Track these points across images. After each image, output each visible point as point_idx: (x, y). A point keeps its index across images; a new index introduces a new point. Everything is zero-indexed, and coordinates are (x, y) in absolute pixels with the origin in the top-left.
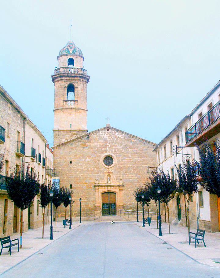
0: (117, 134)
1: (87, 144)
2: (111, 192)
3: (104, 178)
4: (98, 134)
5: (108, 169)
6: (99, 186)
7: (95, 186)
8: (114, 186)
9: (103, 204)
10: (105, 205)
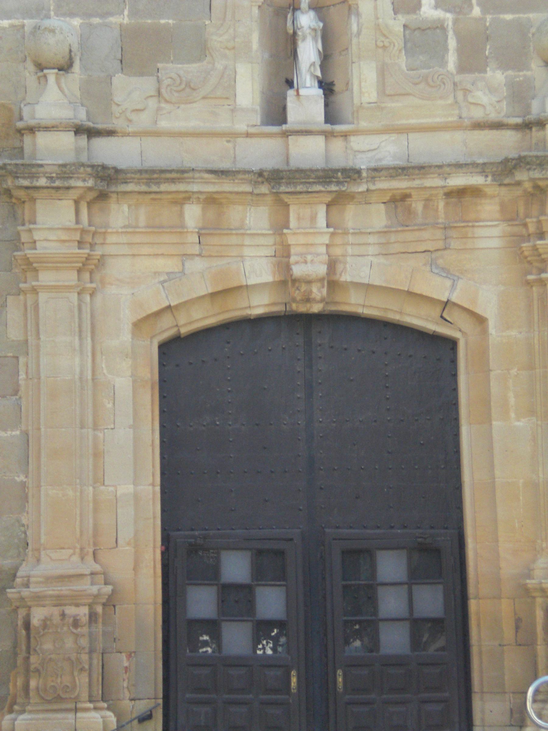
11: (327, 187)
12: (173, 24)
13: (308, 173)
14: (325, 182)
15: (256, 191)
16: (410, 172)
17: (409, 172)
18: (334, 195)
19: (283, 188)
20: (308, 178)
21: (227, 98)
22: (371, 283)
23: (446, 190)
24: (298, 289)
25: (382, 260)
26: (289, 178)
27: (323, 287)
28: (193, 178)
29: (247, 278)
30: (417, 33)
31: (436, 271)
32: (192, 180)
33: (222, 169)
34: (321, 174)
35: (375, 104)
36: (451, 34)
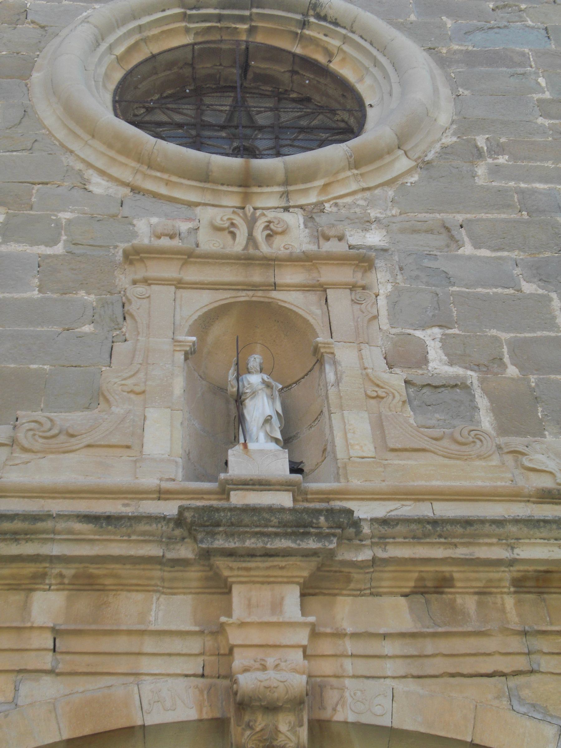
11: (301, 543)
12: (50, 369)
13: (266, 516)
14: (293, 534)
15: (170, 555)
16: (447, 529)
17: (445, 529)
18: (313, 563)
19: (220, 543)
20: (266, 526)
21: (128, 447)
22: (397, 725)
23: (516, 571)
24: (249, 726)
25: (412, 686)
26: (232, 524)
27: (301, 725)
28: (54, 532)
29: (145, 714)
30: (425, 390)
31: (523, 710)
32: (52, 536)
33: (108, 514)
34: (287, 517)
35: (374, 459)
36: (478, 393)
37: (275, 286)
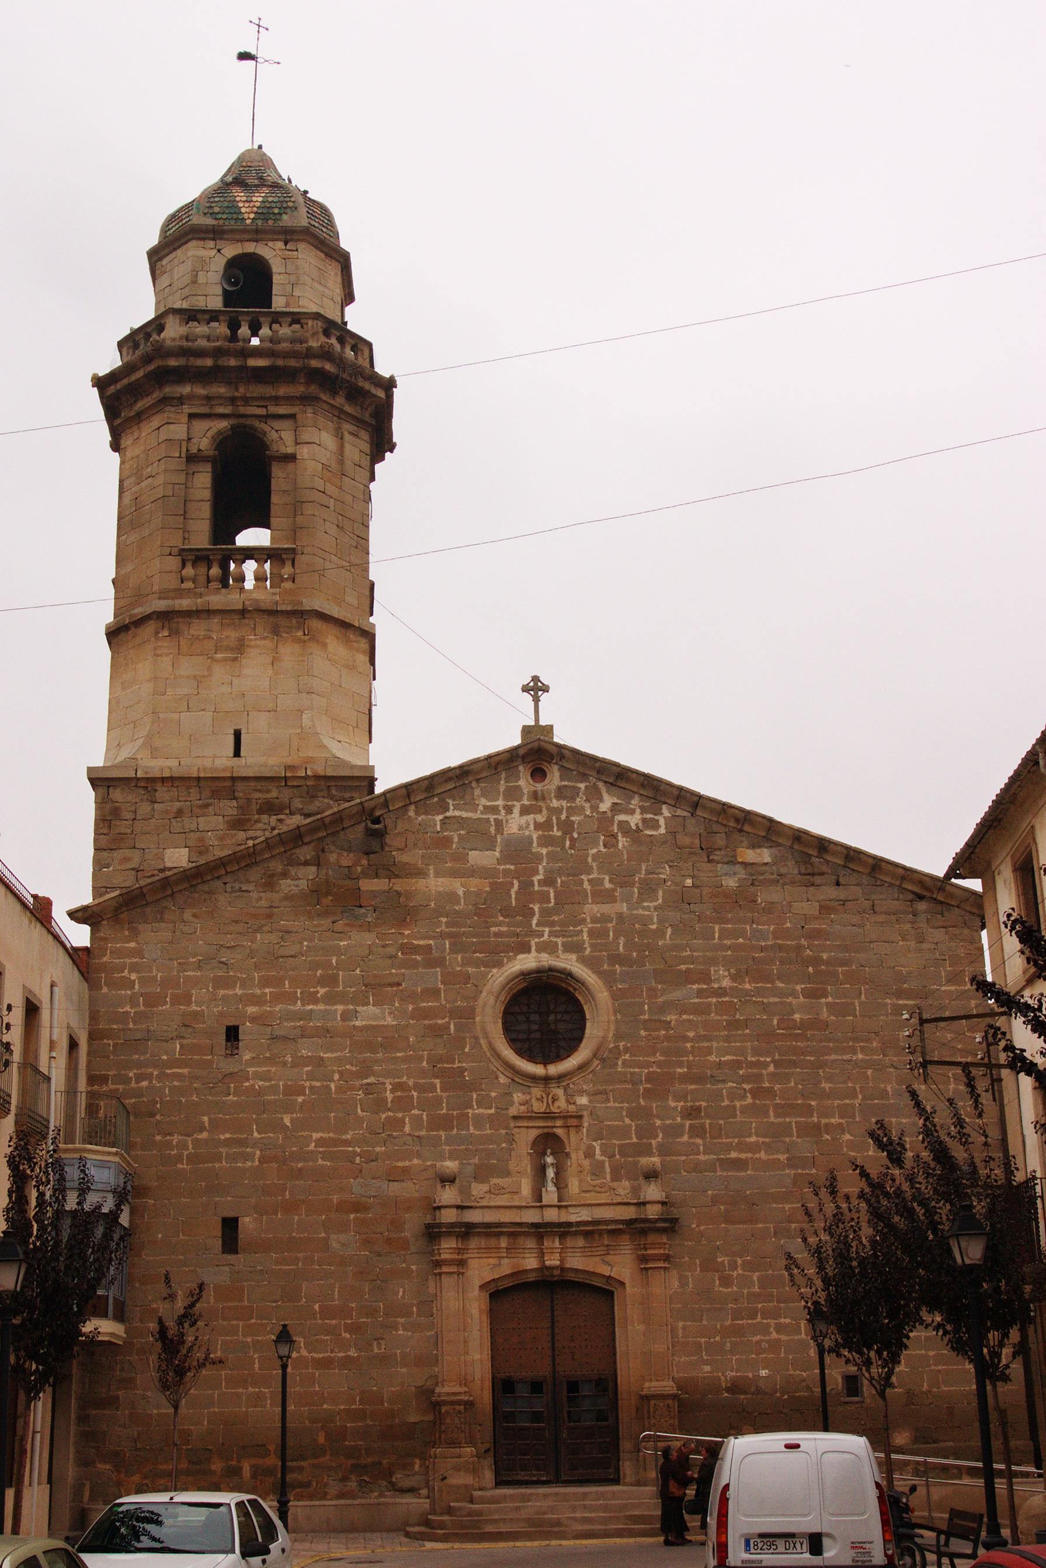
0: (615, 808)
1: (368, 885)
2: (571, 1277)
3: (512, 1165)
4: (456, 808)
5: (537, 1091)
6: (466, 1231)
7: (433, 1233)
8: (590, 1231)
9: (503, 1386)
10: (522, 1391)
37: (555, 1127)
